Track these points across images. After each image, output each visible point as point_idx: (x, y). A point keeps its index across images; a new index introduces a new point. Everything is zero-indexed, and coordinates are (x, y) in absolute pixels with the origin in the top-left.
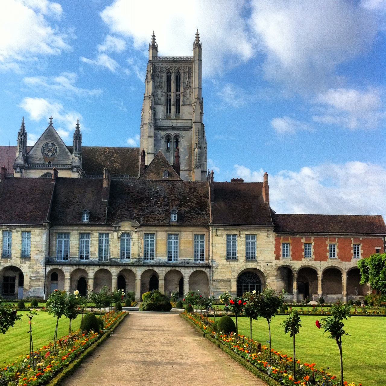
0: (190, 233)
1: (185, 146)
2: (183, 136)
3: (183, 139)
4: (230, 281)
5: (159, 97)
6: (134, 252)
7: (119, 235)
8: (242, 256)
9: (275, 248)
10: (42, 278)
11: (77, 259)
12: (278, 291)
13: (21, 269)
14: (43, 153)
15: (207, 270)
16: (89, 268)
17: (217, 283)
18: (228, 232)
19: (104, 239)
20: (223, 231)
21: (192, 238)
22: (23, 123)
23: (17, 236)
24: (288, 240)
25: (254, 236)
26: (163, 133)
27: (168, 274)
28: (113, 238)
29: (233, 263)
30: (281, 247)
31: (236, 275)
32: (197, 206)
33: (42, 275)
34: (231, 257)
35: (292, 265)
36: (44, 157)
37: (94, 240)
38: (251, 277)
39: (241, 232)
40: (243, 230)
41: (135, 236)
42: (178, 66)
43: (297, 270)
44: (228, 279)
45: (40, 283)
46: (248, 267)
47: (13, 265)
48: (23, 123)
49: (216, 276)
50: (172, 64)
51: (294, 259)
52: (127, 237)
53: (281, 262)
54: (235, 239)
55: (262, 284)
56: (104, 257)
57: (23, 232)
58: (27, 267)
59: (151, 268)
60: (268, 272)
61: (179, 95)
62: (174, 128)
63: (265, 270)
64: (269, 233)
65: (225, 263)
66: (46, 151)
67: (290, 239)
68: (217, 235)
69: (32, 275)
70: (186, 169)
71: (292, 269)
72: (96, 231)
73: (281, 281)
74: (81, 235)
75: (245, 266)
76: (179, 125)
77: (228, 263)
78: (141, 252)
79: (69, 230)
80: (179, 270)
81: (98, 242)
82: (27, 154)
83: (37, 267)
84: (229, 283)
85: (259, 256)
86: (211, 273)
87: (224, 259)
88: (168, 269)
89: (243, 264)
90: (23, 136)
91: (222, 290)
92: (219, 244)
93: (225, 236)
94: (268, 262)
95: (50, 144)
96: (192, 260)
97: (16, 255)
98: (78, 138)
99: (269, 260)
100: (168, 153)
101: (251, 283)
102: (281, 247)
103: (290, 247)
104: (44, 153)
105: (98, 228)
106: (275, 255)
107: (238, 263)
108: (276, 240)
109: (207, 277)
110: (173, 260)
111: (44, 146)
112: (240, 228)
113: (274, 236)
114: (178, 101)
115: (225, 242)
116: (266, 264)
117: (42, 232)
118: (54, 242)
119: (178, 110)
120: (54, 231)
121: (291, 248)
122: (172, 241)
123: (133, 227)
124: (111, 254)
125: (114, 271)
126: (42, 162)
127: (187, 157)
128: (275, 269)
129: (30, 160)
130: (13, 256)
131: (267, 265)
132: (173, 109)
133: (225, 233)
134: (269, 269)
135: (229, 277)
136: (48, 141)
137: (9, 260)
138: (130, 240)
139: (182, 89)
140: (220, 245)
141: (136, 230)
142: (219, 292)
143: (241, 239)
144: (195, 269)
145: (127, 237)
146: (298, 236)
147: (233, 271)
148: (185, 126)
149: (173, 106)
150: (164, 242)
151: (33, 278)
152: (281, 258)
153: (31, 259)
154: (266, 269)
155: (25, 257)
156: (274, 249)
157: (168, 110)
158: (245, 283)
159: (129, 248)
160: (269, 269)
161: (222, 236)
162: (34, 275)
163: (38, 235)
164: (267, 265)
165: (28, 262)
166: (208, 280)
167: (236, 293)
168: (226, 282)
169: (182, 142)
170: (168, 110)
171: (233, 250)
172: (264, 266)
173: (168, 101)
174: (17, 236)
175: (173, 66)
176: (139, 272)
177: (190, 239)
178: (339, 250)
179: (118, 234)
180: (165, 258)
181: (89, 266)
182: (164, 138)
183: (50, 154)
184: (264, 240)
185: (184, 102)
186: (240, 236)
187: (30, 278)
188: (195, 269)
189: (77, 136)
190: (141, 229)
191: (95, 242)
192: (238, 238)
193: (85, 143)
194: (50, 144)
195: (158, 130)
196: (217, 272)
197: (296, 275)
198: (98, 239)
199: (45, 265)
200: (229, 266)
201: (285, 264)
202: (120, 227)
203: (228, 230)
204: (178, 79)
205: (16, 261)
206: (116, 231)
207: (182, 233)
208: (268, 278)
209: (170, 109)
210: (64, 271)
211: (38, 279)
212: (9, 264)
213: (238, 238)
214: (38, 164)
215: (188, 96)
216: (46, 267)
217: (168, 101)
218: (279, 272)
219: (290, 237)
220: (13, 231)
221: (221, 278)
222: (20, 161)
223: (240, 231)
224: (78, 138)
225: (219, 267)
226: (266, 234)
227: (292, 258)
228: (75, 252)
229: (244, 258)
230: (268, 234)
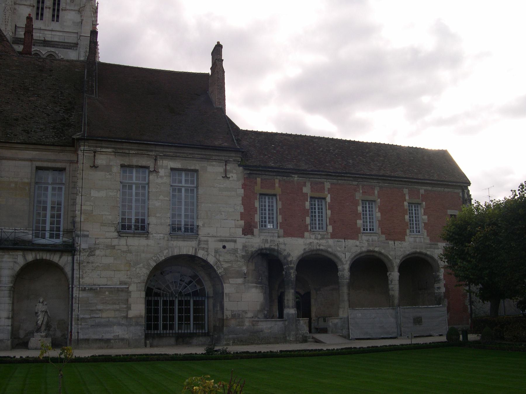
0: (28, 163)
4: (127, 291)
15: (64, 261)
17: (90, 295)
18: (126, 161)
20: (112, 157)
29: (136, 242)
31: (144, 272)
39: (160, 162)
40: (166, 157)
44: (121, 283)
49: (90, 277)
55: (208, 297)
59: (40, 256)
65: (115, 242)
68: (94, 167)
76: (56, 39)
77: (123, 241)
85: (204, 225)
86: (76, 267)
87: (113, 229)
88: (20, 260)
91: (104, 315)
93: (116, 169)
107: (151, 242)
109: (67, 280)
119: (56, 17)
133: (116, 162)
135: (124, 278)
142: (97, 320)
143: (159, 181)
148: (66, 41)
161: (108, 168)
166: (69, 288)
167: (143, 321)
168: (118, 290)
172: (216, 251)
177: (26, 181)
186: (155, 171)
188: (30, 257)
195: (18, 44)
200: (125, 248)
221: (103, 281)
223: (156, 160)
225: (97, 252)
229: (168, 229)
230: (226, 171)
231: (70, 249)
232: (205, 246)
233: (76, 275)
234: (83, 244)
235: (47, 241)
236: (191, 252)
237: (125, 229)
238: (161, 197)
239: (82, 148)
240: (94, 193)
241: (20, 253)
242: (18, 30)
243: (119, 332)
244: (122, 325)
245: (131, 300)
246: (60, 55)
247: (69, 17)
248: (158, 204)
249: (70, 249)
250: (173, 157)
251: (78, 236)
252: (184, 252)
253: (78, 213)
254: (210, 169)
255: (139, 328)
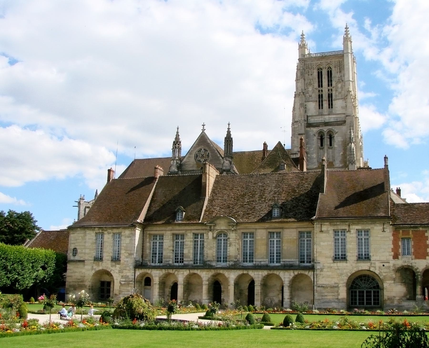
0: (295, 230)
1: (339, 142)
2: (337, 131)
3: (336, 135)
4: (338, 287)
5: (310, 94)
6: (231, 254)
7: (215, 235)
8: (353, 256)
9: (392, 245)
10: (131, 283)
11: (171, 262)
12: (397, 298)
13: (111, 272)
14: (196, 160)
15: (310, 274)
16: (178, 272)
17: (322, 289)
18: (335, 228)
19: (199, 240)
20: (329, 226)
21: (296, 236)
22: (177, 132)
23: (109, 238)
24: (408, 234)
25: (367, 232)
26: (315, 130)
27: (295, 278)
28: (208, 239)
29: (341, 265)
30: (400, 243)
31: (345, 279)
32: (306, 199)
33: (131, 279)
34: (340, 257)
35: (414, 264)
36: (197, 164)
37: (189, 241)
38: (365, 280)
40: (354, 224)
41: (232, 236)
42: (329, 61)
43: (421, 270)
45: (129, 288)
46: (360, 269)
47: (105, 268)
48: (177, 132)
50: (322, 60)
51: (417, 258)
52: (224, 237)
53: (400, 262)
54: (345, 235)
56: (198, 260)
57: (114, 234)
58: (117, 271)
60: (384, 274)
61: (332, 90)
62: (326, 124)
63: (381, 272)
64: (385, 226)
66: (198, 157)
67: (411, 233)
68: (321, 231)
69: (122, 280)
70: (341, 166)
71: (414, 270)
72: (189, 231)
73: (401, 285)
74: (176, 236)
75: (356, 267)
76: (332, 120)
77: (335, 265)
78: (239, 254)
79: (162, 230)
80: (278, 274)
81: (192, 243)
82: (181, 161)
83: (126, 271)
84: (336, 289)
85: (373, 256)
86: (315, 277)
87: (331, 259)
89: (354, 265)
90: (177, 143)
91: (328, 297)
92: (324, 242)
93: (331, 232)
94: (384, 263)
95: (203, 150)
96: (297, 263)
97: (107, 258)
98: (229, 142)
99: (385, 259)
100: (321, 151)
101: (367, 288)
102: (400, 243)
103: (412, 243)
104: (198, 159)
105: (193, 228)
106: (393, 253)
107: (348, 264)
108: (393, 235)
110: (275, 262)
111: (197, 153)
112: (349, 222)
113: (391, 230)
114: (330, 96)
115: (332, 239)
116: (382, 264)
117: (132, 233)
118: (148, 244)
119: (331, 105)
120: (148, 232)
121: (413, 244)
122: (273, 241)
123: (230, 225)
124: (205, 257)
125: (205, 275)
126: (194, 169)
127: (342, 153)
128: (393, 270)
129: (184, 167)
130: (104, 259)
131: (384, 266)
132: (326, 104)
134: (385, 270)
136: (201, 147)
137: (100, 263)
138: (227, 240)
139: (334, 83)
140: (326, 243)
141: (233, 229)
142: (325, 300)
143: (351, 235)
144: (296, 273)
145: (224, 237)
146: (421, 229)
147: (341, 274)
148: (338, 120)
149: (325, 102)
150: (265, 242)
151: (123, 283)
152: (400, 257)
153: (121, 262)
154: (382, 271)
155: (116, 260)
156: (392, 246)
157: (321, 106)
158: (359, 288)
159: (226, 249)
160: (385, 270)
161: (327, 232)
162: (124, 280)
163: (128, 237)
164: (384, 266)
165: (118, 266)
168: (334, 287)
169: (335, 138)
170: (321, 106)
171: (365, 251)
172: (380, 268)
173: (320, 97)
174: (109, 238)
175: (323, 61)
176: (232, 276)
177: (295, 238)
178: (394, 237)
179: (213, 234)
180: (265, 260)
181: (178, 270)
182: (317, 135)
183: (202, 160)
184: (379, 236)
185: (336, 96)
186: (349, 231)
187: (120, 283)
188: (296, 273)
189: (229, 140)
190: (238, 228)
191: (189, 243)
192: (348, 234)
193: (236, 148)
194: (203, 150)
196: (321, 276)
197: (420, 279)
198: (192, 240)
199: (134, 269)
200: (336, 268)
201: (406, 264)
202: (214, 226)
203: (335, 225)
204: (330, 74)
205: (106, 265)
206: (211, 230)
207: (285, 230)
208: (385, 282)
209: (322, 105)
210: (154, 275)
211: (127, 283)
212: (100, 268)
213: (348, 234)
214: (190, 171)
215: (340, 90)
216: (135, 270)
217: (320, 97)
218: (398, 274)
219: (411, 231)
220: (105, 232)
221: (327, 283)
222: (174, 169)
223: (349, 226)
224: (229, 142)
225: (324, 270)
226: (381, 228)
227: (413, 257)
228: (169, 254)
229: (355, 258)
230: (384, 229)
231: (312, 268)
232: (374, 265)
233: (315, 280)
234: (318, 267)
235: (306, 264)
236: (367, 268)
237: (336, 258)
238: (352, 243)
239: (315, 223)
240: (322, 244)
241: (292, 271)
242: (309, 118)
243: (334, 305)
244: (336, 302)
245: (339, 291)
246: (335, 130)
247: (338, 104)
248: (351, 246)
249: (312, 268)
250: (358, 224)
251: (316, 263)
252: (364, 268)
253: (315, 253)
254: (375, 228)
255: (344, 303)
